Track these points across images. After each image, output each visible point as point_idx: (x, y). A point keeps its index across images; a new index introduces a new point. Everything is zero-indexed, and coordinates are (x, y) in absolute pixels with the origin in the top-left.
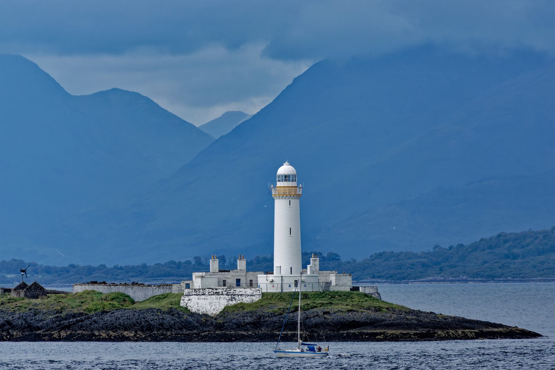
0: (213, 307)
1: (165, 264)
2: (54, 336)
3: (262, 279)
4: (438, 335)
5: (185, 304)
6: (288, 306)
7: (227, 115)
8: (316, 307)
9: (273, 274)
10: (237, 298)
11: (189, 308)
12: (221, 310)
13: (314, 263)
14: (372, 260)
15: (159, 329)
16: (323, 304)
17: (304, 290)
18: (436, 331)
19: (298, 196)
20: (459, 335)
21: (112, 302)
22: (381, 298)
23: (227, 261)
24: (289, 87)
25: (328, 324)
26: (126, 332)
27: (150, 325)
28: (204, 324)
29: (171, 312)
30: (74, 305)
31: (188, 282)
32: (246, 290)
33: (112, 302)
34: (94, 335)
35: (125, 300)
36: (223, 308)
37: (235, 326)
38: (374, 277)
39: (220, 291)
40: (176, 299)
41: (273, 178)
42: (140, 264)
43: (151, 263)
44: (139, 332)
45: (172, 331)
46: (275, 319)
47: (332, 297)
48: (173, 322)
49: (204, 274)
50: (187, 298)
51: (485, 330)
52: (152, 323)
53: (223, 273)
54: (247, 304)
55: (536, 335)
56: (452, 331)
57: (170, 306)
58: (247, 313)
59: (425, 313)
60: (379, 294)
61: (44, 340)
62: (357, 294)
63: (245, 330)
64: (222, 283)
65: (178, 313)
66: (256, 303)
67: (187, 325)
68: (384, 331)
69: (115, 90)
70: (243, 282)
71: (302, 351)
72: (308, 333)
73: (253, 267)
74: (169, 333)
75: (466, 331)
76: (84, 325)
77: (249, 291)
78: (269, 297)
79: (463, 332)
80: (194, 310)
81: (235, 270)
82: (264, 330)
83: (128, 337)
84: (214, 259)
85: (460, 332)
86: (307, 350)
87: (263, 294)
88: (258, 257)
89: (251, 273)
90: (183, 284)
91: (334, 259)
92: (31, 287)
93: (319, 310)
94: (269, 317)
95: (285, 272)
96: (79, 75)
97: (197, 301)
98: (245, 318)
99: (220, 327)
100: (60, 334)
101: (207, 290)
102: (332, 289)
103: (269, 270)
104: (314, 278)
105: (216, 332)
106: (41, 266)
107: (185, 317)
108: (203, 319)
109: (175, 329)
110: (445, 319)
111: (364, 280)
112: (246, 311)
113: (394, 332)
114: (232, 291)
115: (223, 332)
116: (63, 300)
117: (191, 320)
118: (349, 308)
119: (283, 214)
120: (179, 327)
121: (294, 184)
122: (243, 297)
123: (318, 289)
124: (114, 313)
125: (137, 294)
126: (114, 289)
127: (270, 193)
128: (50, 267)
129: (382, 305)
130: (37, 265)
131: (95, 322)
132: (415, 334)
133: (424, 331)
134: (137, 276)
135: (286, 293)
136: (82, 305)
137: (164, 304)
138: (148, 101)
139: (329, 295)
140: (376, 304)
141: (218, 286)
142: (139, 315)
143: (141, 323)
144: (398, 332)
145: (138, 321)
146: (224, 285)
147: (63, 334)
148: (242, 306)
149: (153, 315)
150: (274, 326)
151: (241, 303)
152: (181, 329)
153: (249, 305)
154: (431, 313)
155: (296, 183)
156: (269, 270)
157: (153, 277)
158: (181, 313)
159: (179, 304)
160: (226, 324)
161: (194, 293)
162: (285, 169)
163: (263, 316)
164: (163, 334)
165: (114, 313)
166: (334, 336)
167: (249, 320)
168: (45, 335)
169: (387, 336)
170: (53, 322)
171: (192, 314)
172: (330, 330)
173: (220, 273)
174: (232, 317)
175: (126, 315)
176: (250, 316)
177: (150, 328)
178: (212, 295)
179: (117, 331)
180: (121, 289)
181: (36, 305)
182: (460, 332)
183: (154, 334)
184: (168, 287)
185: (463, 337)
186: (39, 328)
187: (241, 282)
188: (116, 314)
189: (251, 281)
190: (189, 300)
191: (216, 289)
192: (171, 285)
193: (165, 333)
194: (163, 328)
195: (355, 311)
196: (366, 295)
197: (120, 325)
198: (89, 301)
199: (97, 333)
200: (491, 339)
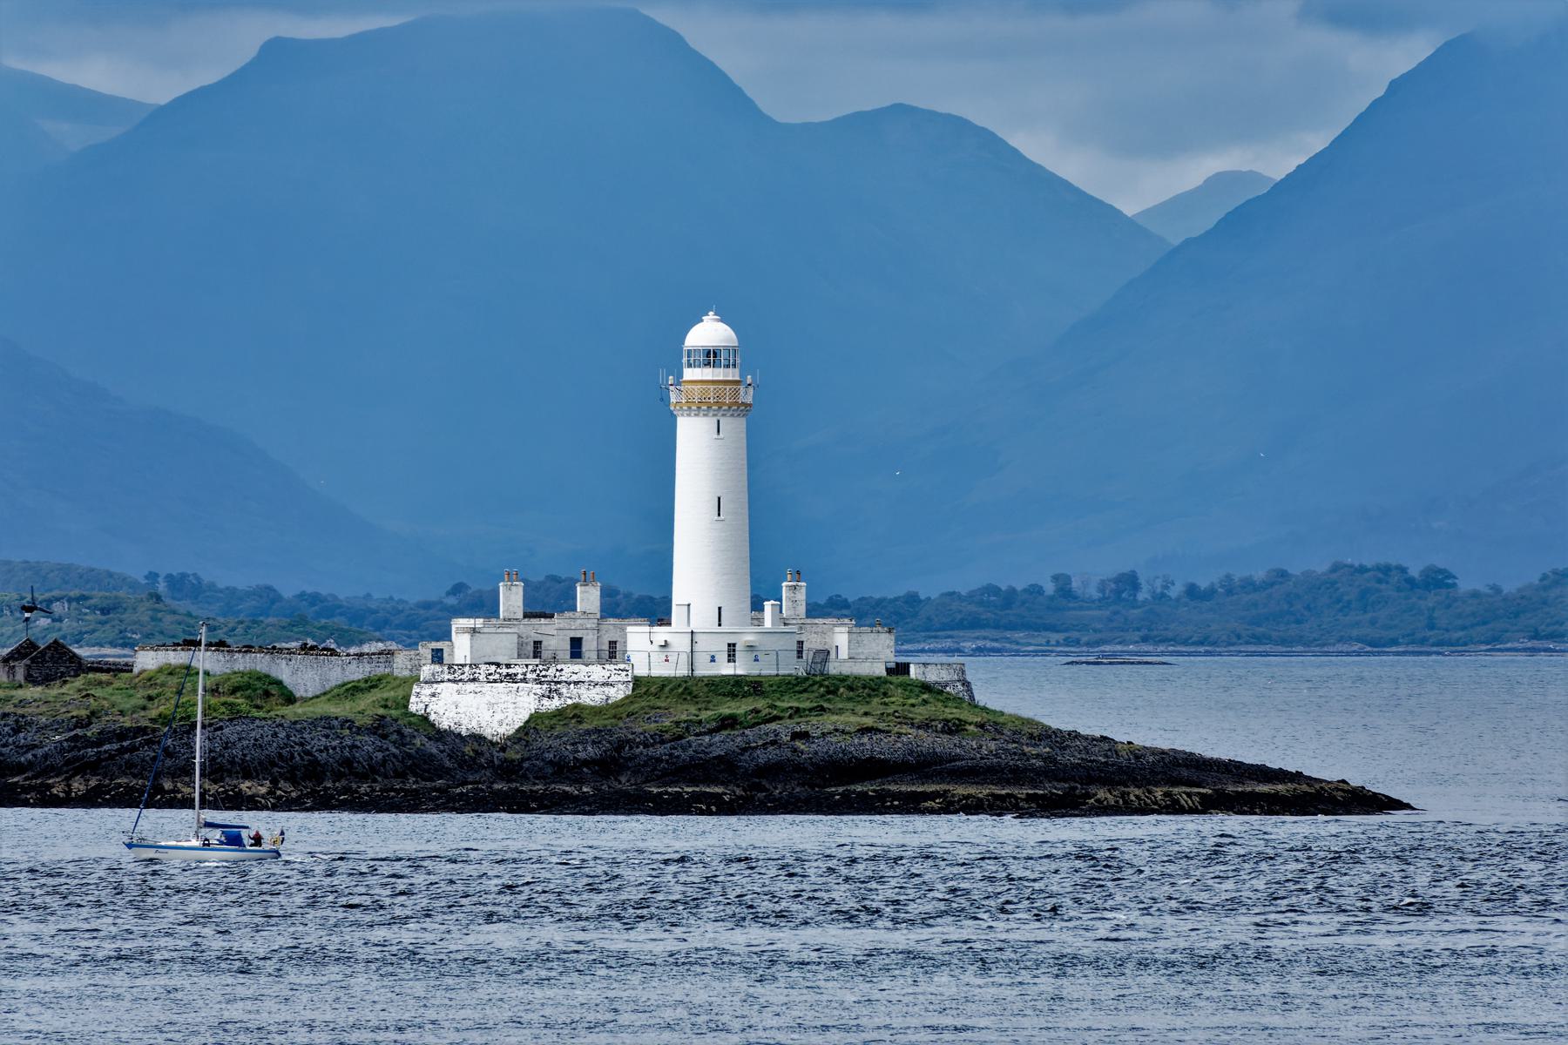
0: (499, 716)
1: (971, 595)
2: (54, 791)
3: (640, 640)
4: (1098, 801)
5: (422, 706)
6: (704, 715)
7: (1218, 182)
9: (669, 624)
10: (564, 690)
11: (432, 717)
13: (793, 597)
14: (1545, 588)
16: (798, 710)
17: (755, 672)
18: (1092, 789)
19: (742, 409)
20: (1155, 803)
21: (231, 699)
22: (972, 697)
23: (1145, 587)
24: (1376, 103)
25: (799, 768)
26: (248, 784)
27: (315, 762)
29: (379, 727)
30: (127, 705)
31: (438, 645)
32: (591, 668)
33: (231, 699)
34: (161, 790)
35: (267, 694)
36: (527, 717)
37: (550, 770)
38: (1536, 636)
39: (519, 670)
40: (400, 693)
41: (673, 357)
44: (282, 784)
45: (375, 781)
46: (660, 750)
47: (829, 692)
48: (380, 755)
49: (479, 622)
50: (427, 690)
51: (1231, 788)
52: (322, 757)
53: (534, 621)
54: (592, 708)
57: (381, 711)
58: (588, 732)
59: (1086, 738)
60: (966, 684)
61: (26, 804)
62: (900, 685)
63: (572, 782)
64: (530, 648)
65: (399, 732)
66: (617, 705)
67: (422, 765)
70: (589, 646)
71: (206, 845)
72: (739, 792)
73: (617, 607)
74: (364, 788)
75: (1176, 790)
76: (136, 760)
77: (598, 672)
79: (1166, 794)
80: (445, 723)
81: (567, 614)
82: (625, 783)
83: (253, 796)
85: (1159, 793)
86: (222, 843)
87: (637, 682)
88: (1228, 577)
89: (612, 621)
90: (425, 650)
91: (1440, 584)
92: (43, 653)
93: (784, 729)
94: (646, 746)
95: (702, 619)
97: (456, 697)
98: (580, 748)
99: (508, 770)
100: (69, 786)
101: (484, 667)
102: (833, 669)
103: (658, 612)
106: (628, 596)
107: (417, 742)
108: (467, 749)
109: (386, 776)
110: (1137, 757)
111: (1509, 645)
112: (585, 726)
113: (972, 790)
114: (552, 672)
115: (514, 785)
116: (98, 692)
117: (434, 751)
118: (868, 721)
119: (700, 455)
120: (395, 771)
121: (732, 374)
122: (582, 690)
123: (793, 668)
124: (221, 728)
125: (304, 677)
126: (243, 663)
127: (665, 399)
128: (651, 599)
129: (965, 715)
130: (618, 593)
131: (168, 753)
132: (1030, 798)
133: (1058, 789)
135: (701, 679)
136: (149, 705)
137: (365, 707)
138: (989, 141)
139: (821, 686)
140: (951, 713)
141: (519, 656)
142: (288, 737)
143: (293, 757)
144: (982, 792)
145: (284, 752)
146: (537, 654)
147: (78, 786)
148: (576, 713)
149: (327, 736)
150: (655, 769)
151: (576, 706)
152: (402, 775)
153: (596, 711)
154: (1104, 739)
155: (737, 370)
156: (658, 612)
157: (928, 630)
158: (407, 731)
159: (406, 707)
160: (526, 765)
161: (447, 677)
162: (709, 332)
163: (628, 741)
164: (346, 790)
165: (221, 728)
167: (590, 751)
168: (26, 790)
169: (952, 803)
170: (62, 750)
171: (440, 735)
172: (803, 785)
173: (526, 621)
174: (547, 742)
175: (253, 734)
176: (594, 742)
178: (495, 681)
179: (222, 780)
180: (259, 663)
181: (22, 703)
182: (1159, 793)
183: (326, 789)
185: (1167, 807)
186: (20, 769)
188: (226, 731)
189: (613, 644)
190: (433, 695)
192: (391, 653)
193: (354, 786)
195: (881, 731)
196: (926, 687)
197: (232, 763)
198: (169, 695)
199: (168, 785)
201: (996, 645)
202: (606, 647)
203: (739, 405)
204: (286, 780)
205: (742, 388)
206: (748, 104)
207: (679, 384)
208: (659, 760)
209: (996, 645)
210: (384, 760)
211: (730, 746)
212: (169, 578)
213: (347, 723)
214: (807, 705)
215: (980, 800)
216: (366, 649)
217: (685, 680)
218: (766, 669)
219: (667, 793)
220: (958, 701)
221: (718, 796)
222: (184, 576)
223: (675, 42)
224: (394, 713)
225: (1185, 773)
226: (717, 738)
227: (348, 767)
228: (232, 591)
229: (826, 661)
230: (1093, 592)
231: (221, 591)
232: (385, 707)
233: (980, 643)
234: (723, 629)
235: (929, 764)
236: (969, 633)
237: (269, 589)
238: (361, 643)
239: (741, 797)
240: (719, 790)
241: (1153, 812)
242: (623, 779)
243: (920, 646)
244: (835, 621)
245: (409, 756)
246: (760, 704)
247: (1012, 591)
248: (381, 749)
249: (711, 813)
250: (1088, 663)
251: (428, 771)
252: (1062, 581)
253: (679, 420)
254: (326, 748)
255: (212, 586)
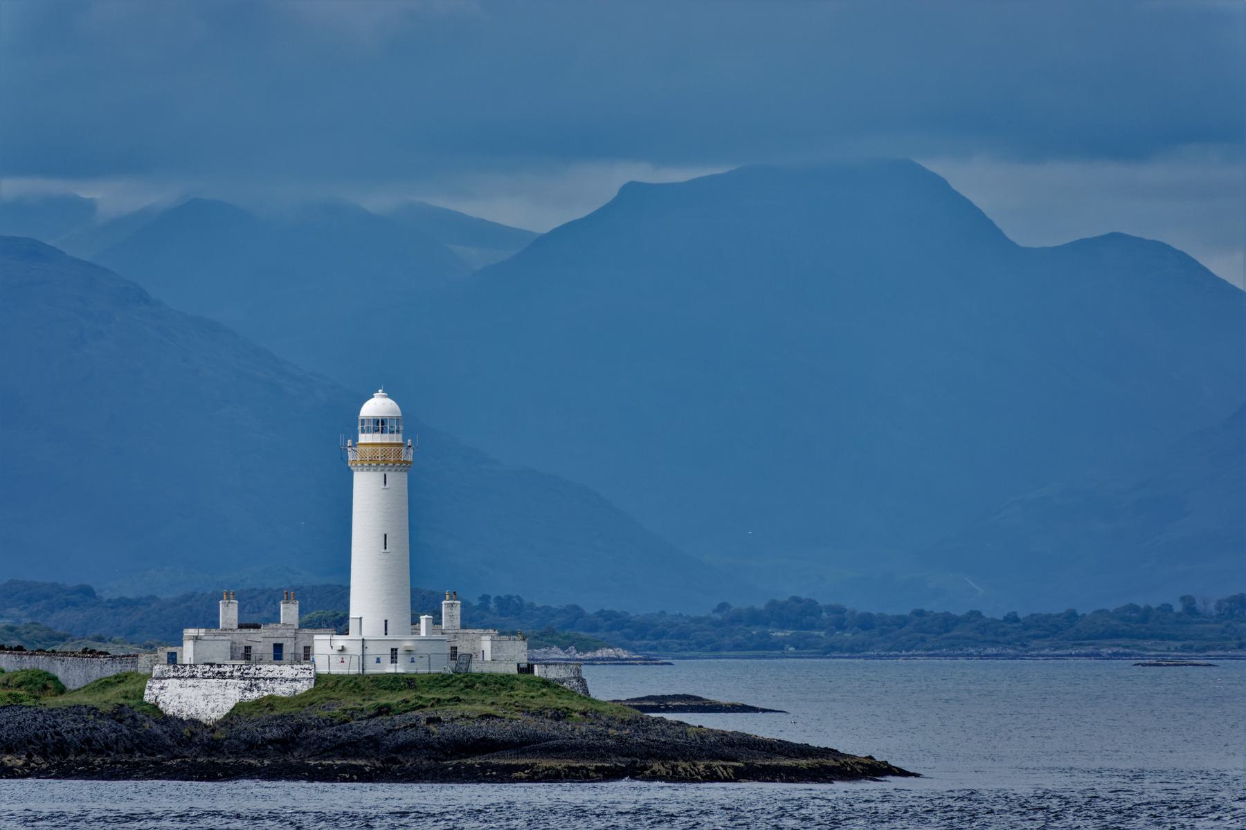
0: (211, 705)
3: (325, 645)
8: (422, 707)
9: (346, 632)
11: (161, 706)
12: (226, 711)
13: (451, 612)
15: (82, 751)
16: (439, 700)
17: (413, 671)
18: (649, 763)
20: (698, 774)
22: (586, 691)
25: (428, 746)
26: (9, 757)
27: (63, 741)
28: (188, 742)
29: (118, 714)
35: (45, 687)
39: (227, 669)
40: (139, 686)
41: (352, 424)
42: (1063, 611)
43: (1085, 609)
44: (35, 758)
45: (108, 755)
47: (467, 687)
48: (114, 735)
49: (202, 632)
50: (157, 685)
52: (69, 737)
53: (245, 631)
55: (875, 770)
56: (685, 765)
57: (122, 701)
58: (275, 718)
60: (582, 681)
62: (525, 681)
65: (133, 718)
67: (147, 744)
68: (533, 761)
69: (1114, 237)
70: (288, 649)
73: (312, 623)
74: (98, 761)
75: (715, 764)
77: (288, 671)
78: (330, 684)
79: (707, 767)
80: (170, 711)
81: (271, 625)
83: (12, 767)
84: (228, 599)
85: (701, 766)
87: (318, 678)
89: (306, 631)
90: (163, 654)
94: (319, 728)
96: (1027, 200)
97: (179, 690)
99: (213, 747)
101: (200, 667)
102: (475, 668)
103: (340, 624)
104: (421, 648)
105: (199, 760)
106: (853, 613)
107: (147, 725)
110: (702, 738)
112: (276, 713)
114: (252, 670)
115: (212, 759)
117: (159, 732)
118: (490, 710)
119: (371, 501)
121: (397, 438)
122: (276, 685)
127: (344, 459)
128: (870, 615)
132: (598, 769)
133: (622, 763)
134: (1046, 636)
135: (368, 676)
137: (112, 696)
139: (463, 680)
142: (45, 720)
148: (270, 703)
149: (75, 721)
151: (270, 697)
152: (129, 751)
153: (286, 701)
155: (400, 436)
156: (340, 624)
159: (142, 698)
161: (172, 674)
162: (377, 406)
166: (427, 771)
167: (275, 733)
169: (536, 773)
171: (166, 720)
174: (244, 725)
177: (61, 748)
180: (41, 663)
182: (701, 766)
184: (130, 660)
187: (285, 651)
190: (162, 688)
191: (219, 666)
193: (91, 759)
194: (90, 750)
196: (546, 683)
200: (792, 781)
201: (1127, 651)
202: (301, 651)
203: (402, 463)
204: (38, 754)
205: (404, 449)
206: (998, 233)
207: (355, 446)
208: (325, 739)
209: (1127, 651)
210: (117, 740)
211: (381, 728)
212: (498, 598)
213: (93, 710)
214: (449, 696)
215: (558, 771)
216: (599, 654)
217: (356, 677)
218: (420, 668)
219: (321, 765)
220: (571, 693)
221: (362, 767)
222: (510, 598)
223: (941, 183)
224: (132, 702)
225: (727, 750)
226: (372, 722)
227: (88, 744)
228: (547, 609)
229: (469, 662)
230: (1212, 607)
231: (538, 609)
232: (126, 697)
233: (1115, 650)
234: (389, 637)
235: (530, 743)
236: (1107, 642)
237: (576, 607)
238: (596, 649)
239: (379, 768)
240: (361, 762)
241: (719, 780)
242: (296, 754)
243: (1068, 652)
244: (481, 631)
245: (138, 736)
246: (409, 695)
247: (1149, 609)
248: (115, 731)
249: (352, 781)
250: (1150, 665)
251: (152, 748)
252: (1188, 602)
253: (356, 474)
254: (72, 730)
255: (531, 605)
